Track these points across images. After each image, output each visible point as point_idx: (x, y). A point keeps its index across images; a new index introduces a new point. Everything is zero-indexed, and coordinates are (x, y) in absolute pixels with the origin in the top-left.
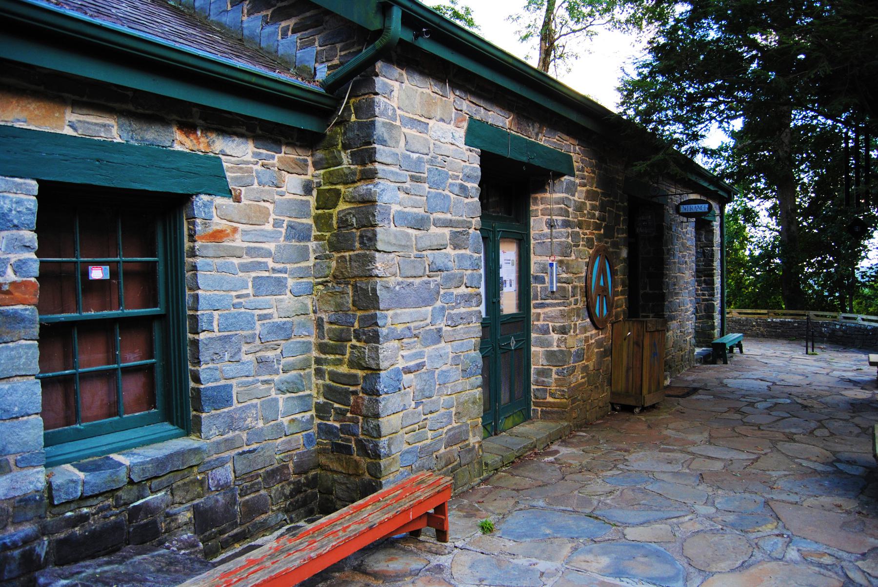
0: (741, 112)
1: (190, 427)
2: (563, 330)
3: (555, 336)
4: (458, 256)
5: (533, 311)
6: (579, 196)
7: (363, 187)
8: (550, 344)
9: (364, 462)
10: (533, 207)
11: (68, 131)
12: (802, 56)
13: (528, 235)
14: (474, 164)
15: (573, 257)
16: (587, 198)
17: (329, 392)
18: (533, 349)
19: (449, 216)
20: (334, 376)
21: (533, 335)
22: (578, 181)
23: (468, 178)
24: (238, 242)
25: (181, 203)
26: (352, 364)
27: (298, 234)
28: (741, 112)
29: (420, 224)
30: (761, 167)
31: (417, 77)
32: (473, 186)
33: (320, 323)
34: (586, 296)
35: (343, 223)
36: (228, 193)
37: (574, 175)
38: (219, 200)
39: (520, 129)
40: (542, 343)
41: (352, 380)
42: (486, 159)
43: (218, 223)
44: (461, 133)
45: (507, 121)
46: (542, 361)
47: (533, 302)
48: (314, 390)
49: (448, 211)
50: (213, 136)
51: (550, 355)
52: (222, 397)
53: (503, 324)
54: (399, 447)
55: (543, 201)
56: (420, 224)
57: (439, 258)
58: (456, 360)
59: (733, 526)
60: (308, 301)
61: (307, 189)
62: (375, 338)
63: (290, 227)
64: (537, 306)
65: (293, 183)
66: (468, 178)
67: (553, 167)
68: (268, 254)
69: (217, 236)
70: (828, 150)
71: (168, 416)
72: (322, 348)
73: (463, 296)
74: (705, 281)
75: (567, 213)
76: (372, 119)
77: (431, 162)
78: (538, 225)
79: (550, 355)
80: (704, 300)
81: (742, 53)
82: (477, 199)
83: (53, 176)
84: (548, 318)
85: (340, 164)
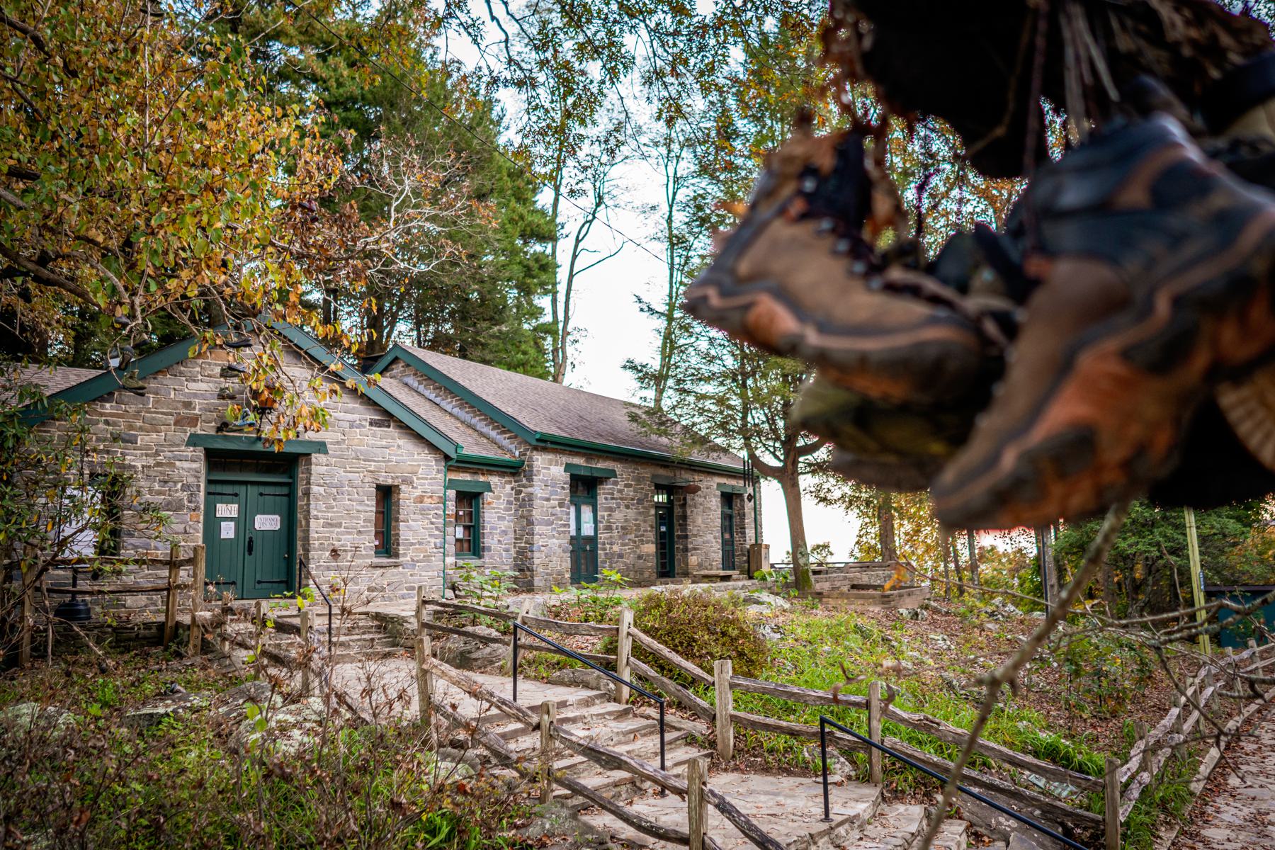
0: (228, 531)
1: (480, 557)
3: (608, 546)
7: (529, 490)
9: (528, 573)
14: (567, 477)
17: (517, 552)
20: (520, 547)
24: (494, 505)
26: (526, 543)
27: (509, 503)
28: (228, 531)
29: (548, 500)
32: (567, 486)
33: (515, 531)
34: (240, 347)
35: (524, 500)
36: (491, 491)
39: (587, 462)
41: (526, 548)
42: (573, 477)
43: (490, 500)
48: (513, 552)
52: (489, 549)
54: (540, 570)
56: (548, 500)
57: (554, 511)
58: (560, 546)
60: (512, 524)
61: (512, 489)
62: (533, 534)
63: (194, 409)
65: (508, 487)
67: (605, 475)
69: (489, 503)
71: (474, 554)
72: (516, 539)
76: (980, 145)
78: (601, 499)
83: (461, 489)
84: (605, 538)
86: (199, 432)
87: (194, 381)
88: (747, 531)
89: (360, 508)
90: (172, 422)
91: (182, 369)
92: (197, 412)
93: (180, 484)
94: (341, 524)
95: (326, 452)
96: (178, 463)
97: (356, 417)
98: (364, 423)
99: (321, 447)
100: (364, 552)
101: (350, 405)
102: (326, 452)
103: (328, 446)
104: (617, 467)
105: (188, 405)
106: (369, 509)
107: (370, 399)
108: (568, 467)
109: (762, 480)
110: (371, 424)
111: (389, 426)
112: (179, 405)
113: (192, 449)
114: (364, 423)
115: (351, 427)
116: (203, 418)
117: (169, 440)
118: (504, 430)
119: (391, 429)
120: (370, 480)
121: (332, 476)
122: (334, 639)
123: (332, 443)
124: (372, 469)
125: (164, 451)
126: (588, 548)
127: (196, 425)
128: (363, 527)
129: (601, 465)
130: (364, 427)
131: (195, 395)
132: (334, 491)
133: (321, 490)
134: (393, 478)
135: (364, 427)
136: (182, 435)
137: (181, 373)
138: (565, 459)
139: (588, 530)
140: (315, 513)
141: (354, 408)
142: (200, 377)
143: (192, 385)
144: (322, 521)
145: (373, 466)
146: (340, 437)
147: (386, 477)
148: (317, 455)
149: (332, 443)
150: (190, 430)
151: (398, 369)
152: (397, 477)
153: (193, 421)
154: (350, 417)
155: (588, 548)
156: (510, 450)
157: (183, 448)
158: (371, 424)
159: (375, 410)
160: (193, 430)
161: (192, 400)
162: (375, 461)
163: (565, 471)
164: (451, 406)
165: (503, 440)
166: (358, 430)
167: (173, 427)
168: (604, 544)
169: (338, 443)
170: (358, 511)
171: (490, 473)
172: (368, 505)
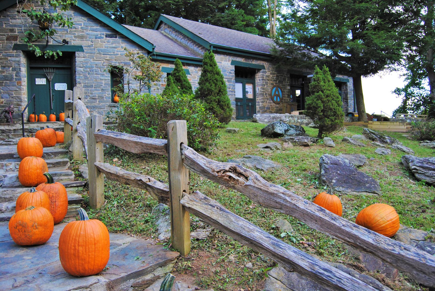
2: (262, 102)
3: (261, 103)
4: (229, 84)
5: (257, 98)
6: (268, 74)
8: (260, 105)
10: (256, 77)
11: (170, 67)
12: (395, 23)
13: (255, 83)
14: (233, 68)
15: (266, 87)
16: (270, 74)
18: (257, 106)
19: (227, 77)
21: (257, 103)
22: (267, 71)
23: (231, 71)
25: (74, 53)
30: (117, 17)
31: (219, 55)
36: (190, 74)
37: (265, 69)
38: (188, 75)
39: (246, 60)
40: (259, 105)
42: (236, 67)
44: (230, 63)
45: (242, 60)
46: (258, 109)
47: (256, 97)
49: (227, 76)
50: (187, 66)
51: (260, 107)
53: (247, 100)
55: (258, 75)
59: (117, 127)
63: (15, 32)
64: (257, 97)
66: (231, 71)
68: (196, 83)
70: (149, 3)
73: (230, 91)
74: (345, 101)
75: (264, 78)
77: (222, 68)
79: (260, 107)
80: (345, 107)
81: (206, 3)
82: (234, 74)
84: (260, 100)
85: (15, 32)
86: (18, 43)
87: (14, 19)
88: (349, 101)
89: (102, 78)
90: (5, 39)
91: (8, 13)
92: (17, 33)
93: (11, 68)
94: (92, 86)
95: (83, 51)
96: (9, 58)
97: (99, 33)
98: (102, 36)
99: (80, 48)
100: (105, 100)
101: (95, 27)
102: (83, 51)
103: (84, 48)
104: (266, 64)
105: (12, 31)
106: (107, 78)
107: (105, 24)
108: (233, 63)
109: (362, 77)
110: (106, 36)
111: (116, 37)
112: (8, 31)
113: (15, 51)
114: (102, 36)
115: (96, 38)
116: (20, 36)
117: (4, 48)
118: (199, 45)
119: (117, 39)
120: (107, 64)
121: (87, 63)
122: (26, 127)
123: (85, 46)
124: (108, 58)
125: (2, 53)
126: (250, 104)
127: (17, 40)
128: (104, 87)
129: (255, 62)
130: (103, 38)
131: (15, 26)
132: (88, 70)
133: (82, 69)
134: (119, 63)
135: (103, 38)
136: (10, 45)
137: (8, 16)
138: (231, 58)
139: (250, 95)
140: (79, 80)
141: (97, 29)
142: (17, 17)
143: (14, 21)
144: (83, 84)
145: (108, 57)
146: (90, 43)
147: (115, 62)
148: (79, 52)
149: (85, 46)
150: (14, 42)
151: (163, 26)
152: (121, 62)
153: (15, 38)
154: (95, 33)
155: (250, 104)
156: (200, 53)
157: (11, 51)
158: (106, 36)
159: (108, 29)
160: (15, 42)
161: (14, 28)
162: (109, 55)
163: (232, 64)
164: (180, 39)
165: (195, 48)
166: (99, 40)
167: (6, 41)
168: (259, 102)
169: (89, 46)
170: (101, 79)
171: (189, 65)
172: (106, 77)
